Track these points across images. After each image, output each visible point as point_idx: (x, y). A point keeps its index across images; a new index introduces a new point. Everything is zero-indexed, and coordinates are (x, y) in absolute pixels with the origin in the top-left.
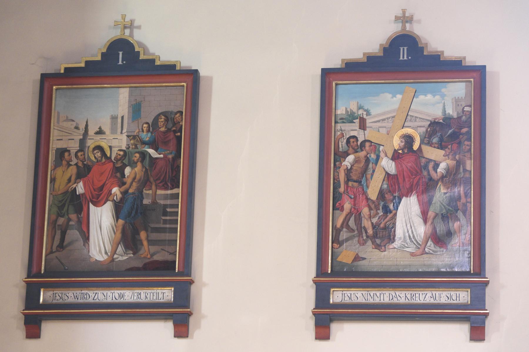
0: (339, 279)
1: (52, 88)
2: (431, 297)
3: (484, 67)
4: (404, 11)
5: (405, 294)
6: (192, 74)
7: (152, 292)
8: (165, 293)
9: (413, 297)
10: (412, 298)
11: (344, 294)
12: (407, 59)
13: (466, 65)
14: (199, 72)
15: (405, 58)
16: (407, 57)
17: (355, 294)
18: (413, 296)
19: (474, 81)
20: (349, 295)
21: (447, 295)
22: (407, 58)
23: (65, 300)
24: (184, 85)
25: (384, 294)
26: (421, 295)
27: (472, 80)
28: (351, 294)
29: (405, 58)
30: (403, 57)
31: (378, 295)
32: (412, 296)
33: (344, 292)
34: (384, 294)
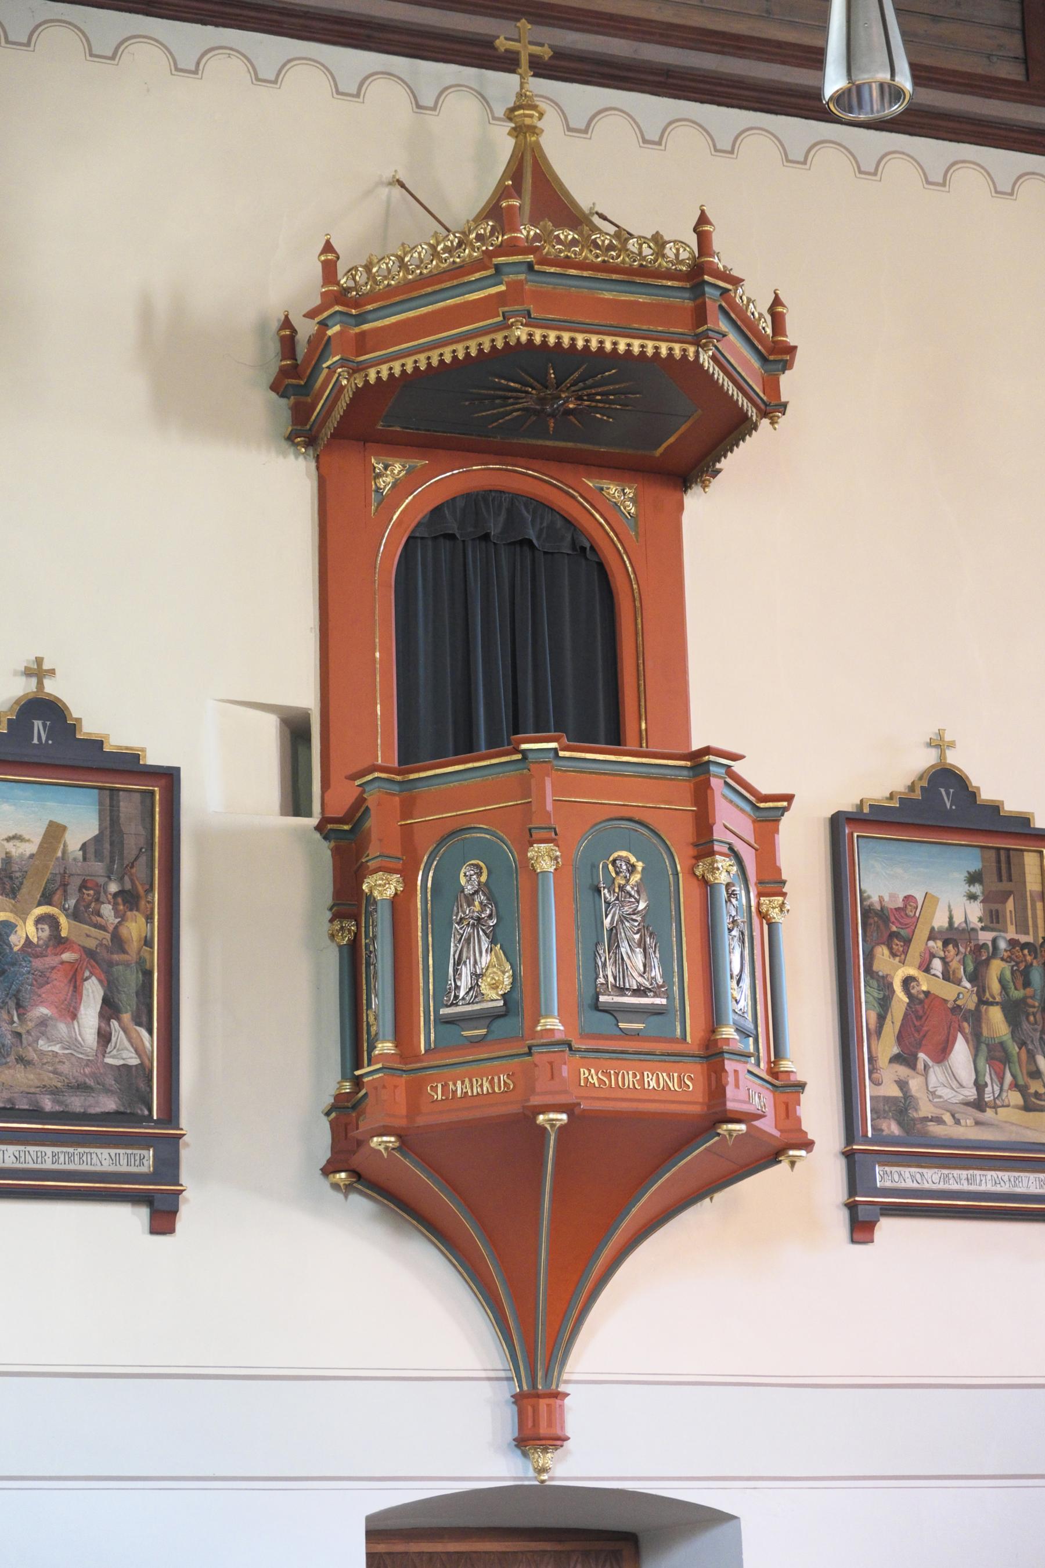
0: (104, 1129)
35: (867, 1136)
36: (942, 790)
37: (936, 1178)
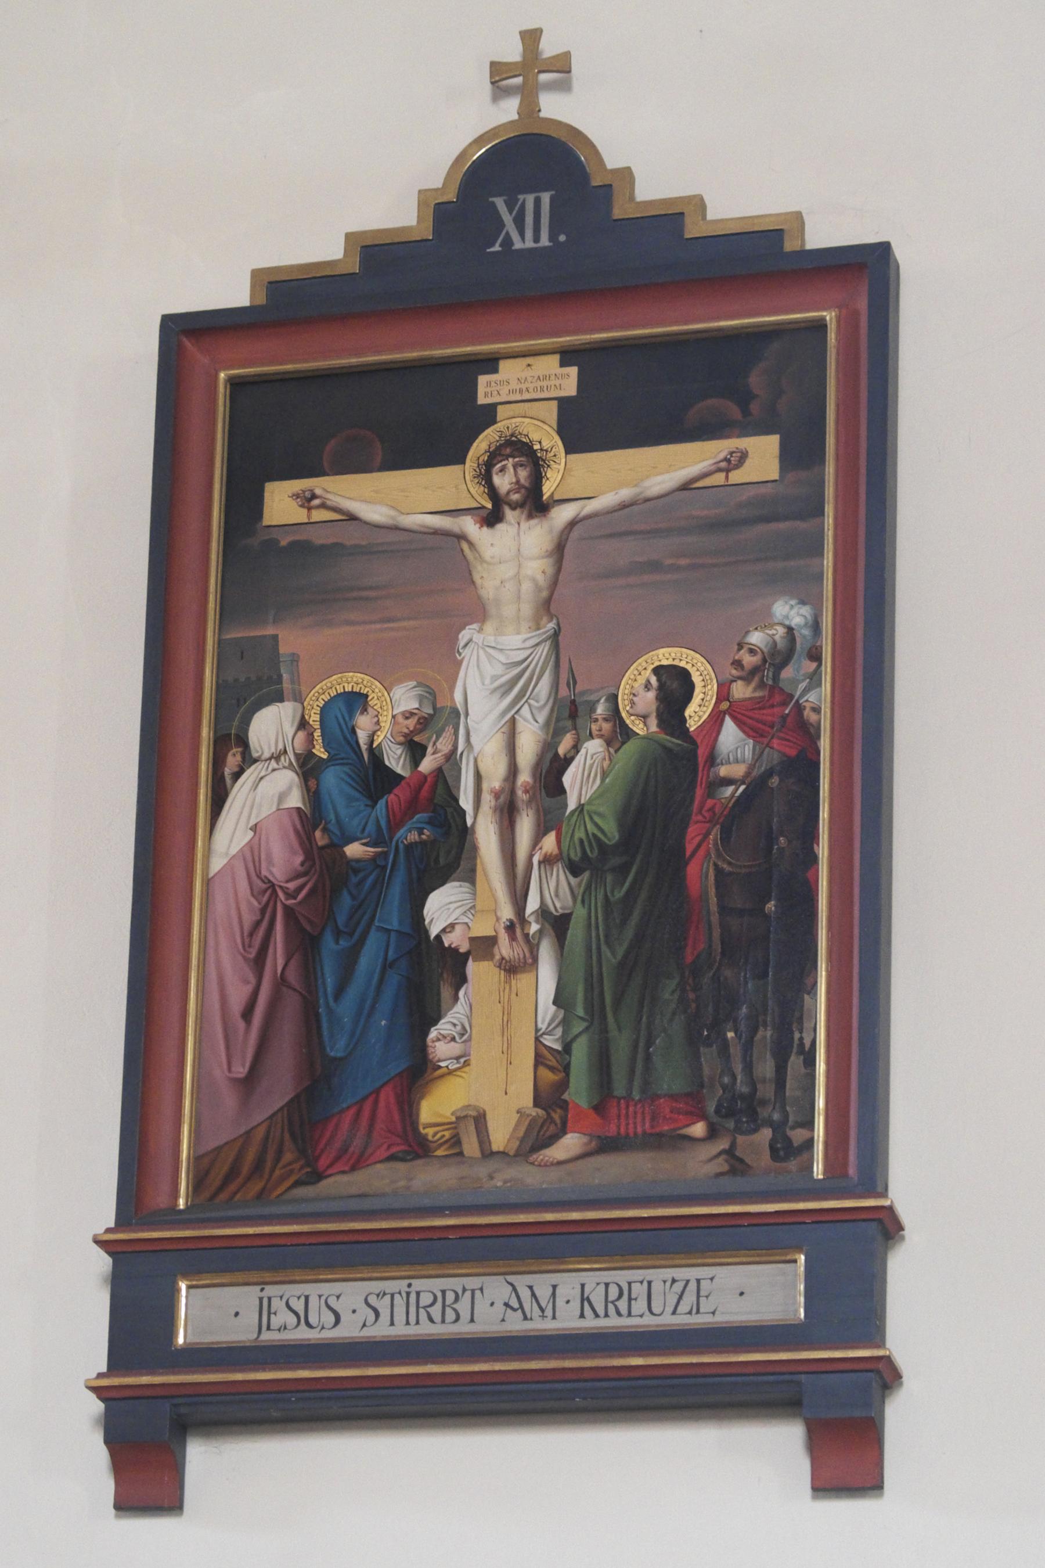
1: (216, 376)
2: (506, 1305)
3: (882, 252)
4: (531, 38)
5: (583, 1286)
6: (861, 267)
7: (400, 1293)
8: (481, 1289)
9: (620, 1304)
10: (448, 1310)
11: (270, 1299)
12: (551, 244)
13: (809, 246)
14: (893, 251)
15: (545, 241)
16: (552, 237)
17: (323, 1299)
18: (457, 1299)
19: (224, 370)
20: (299, 1306)
21: (372, 1300)
22: (550, 240)
23: (323, 1328)
24: (823, 319)
25: (473, 1291)
26: (657, 1287)
27: (829, 316)
28: (307, 1298)
29: (545, 241)
30: (537, 239)
31: (544, 1293)
32: (611, 1298)
33: (267, 1288)
34: (473, 1291)
35: (845, 1175)
36: (500, 203)
37: (265, 1308)
